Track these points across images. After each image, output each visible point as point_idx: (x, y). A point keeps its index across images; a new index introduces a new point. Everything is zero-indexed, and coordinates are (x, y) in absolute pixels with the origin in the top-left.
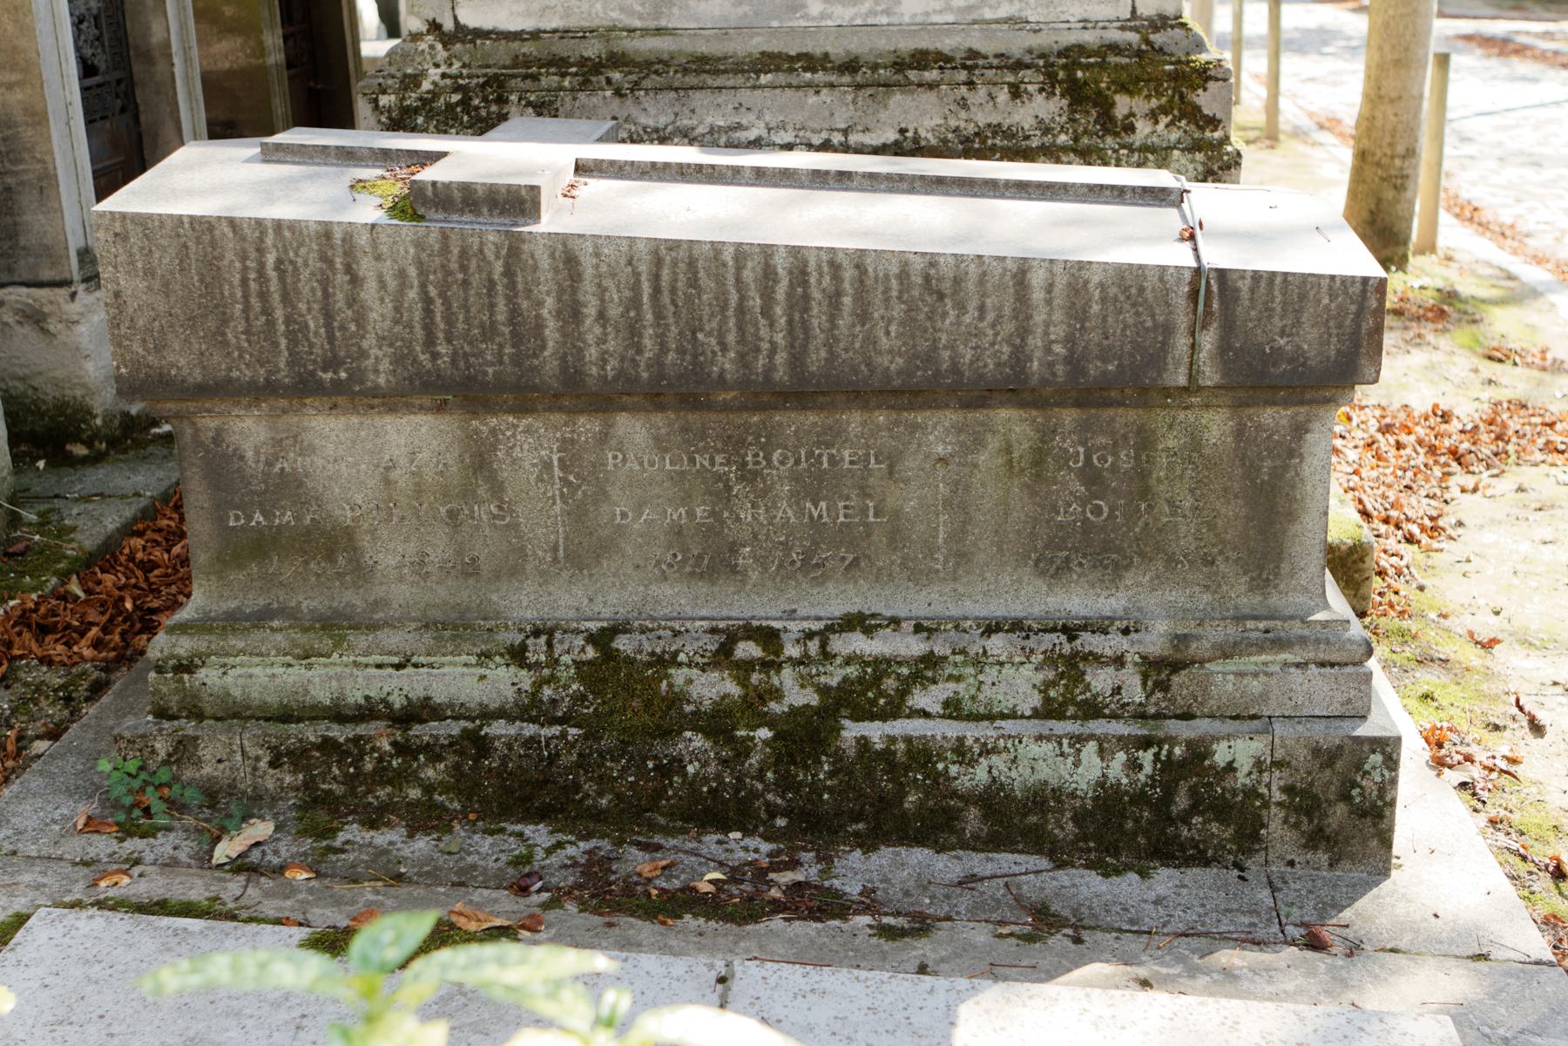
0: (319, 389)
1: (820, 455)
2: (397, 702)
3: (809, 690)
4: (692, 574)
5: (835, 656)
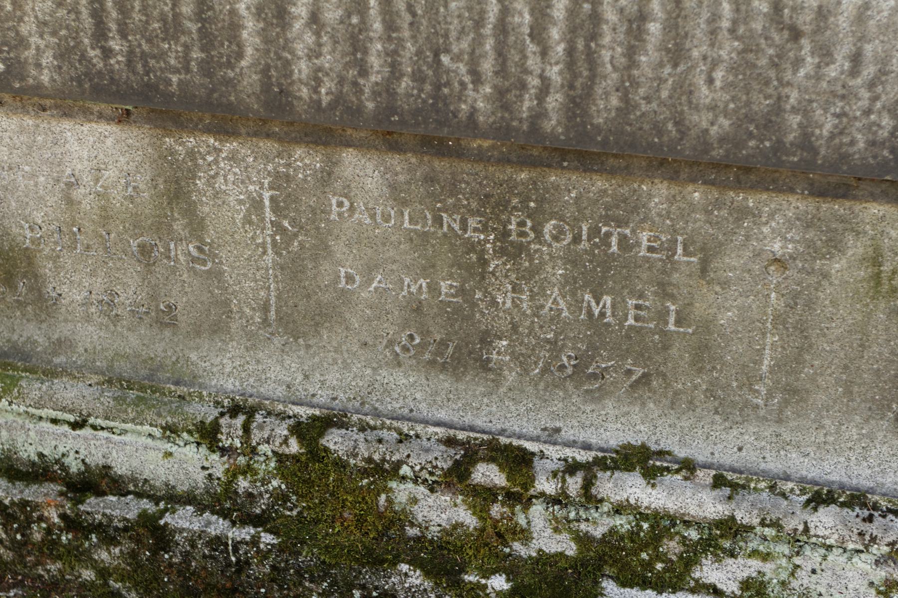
1: (608, 235)
2: (74, 466)
3: (565, 536)
4: (432, 363)
5: (601, 501)
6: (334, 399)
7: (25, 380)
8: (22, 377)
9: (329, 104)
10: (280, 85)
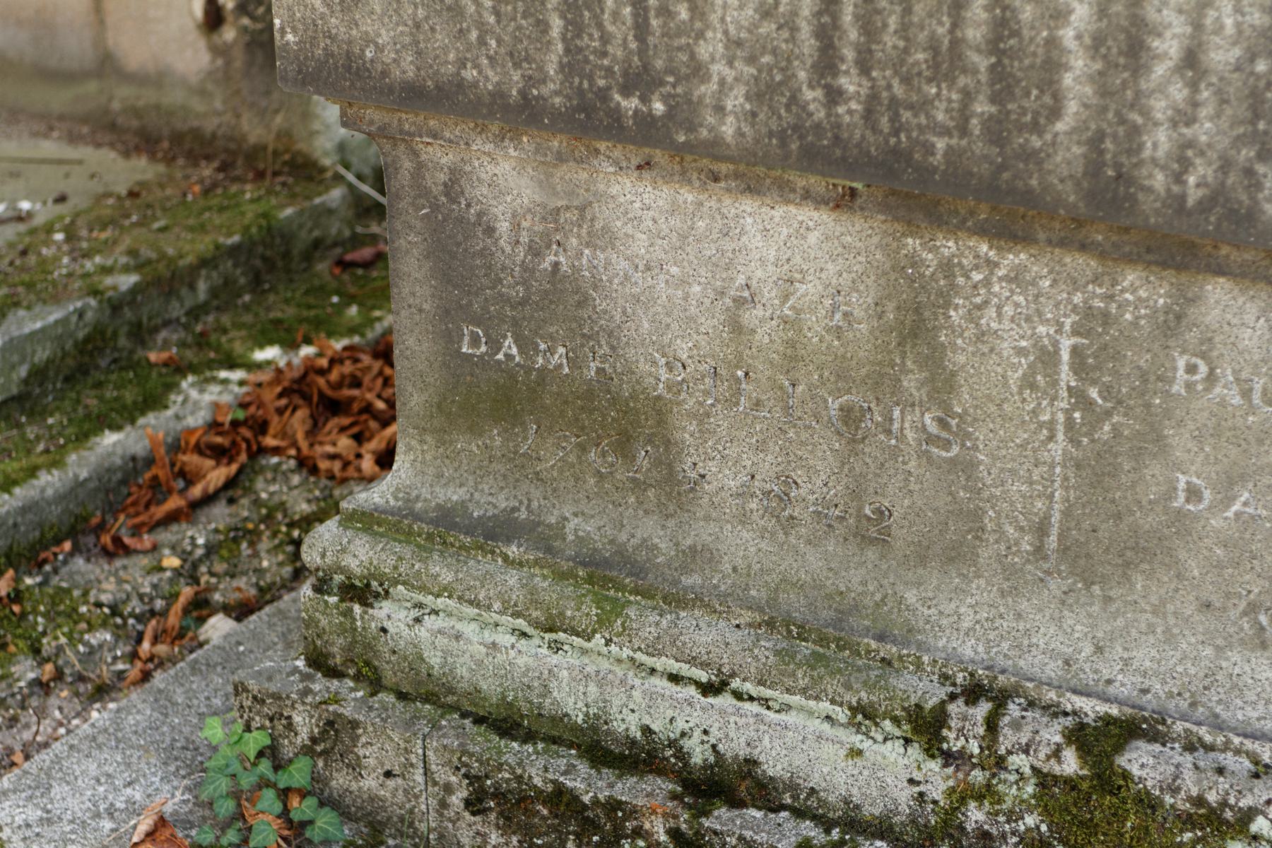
0: (613, 127)
2: (699, 754)
6: (1145, 691)
7: (635, 607)
8: (630, 602)
9: (1200, 202)
10: (1117, 166)
